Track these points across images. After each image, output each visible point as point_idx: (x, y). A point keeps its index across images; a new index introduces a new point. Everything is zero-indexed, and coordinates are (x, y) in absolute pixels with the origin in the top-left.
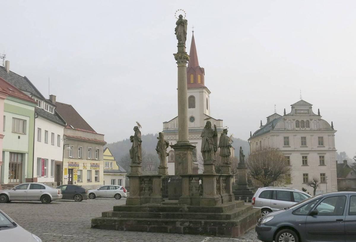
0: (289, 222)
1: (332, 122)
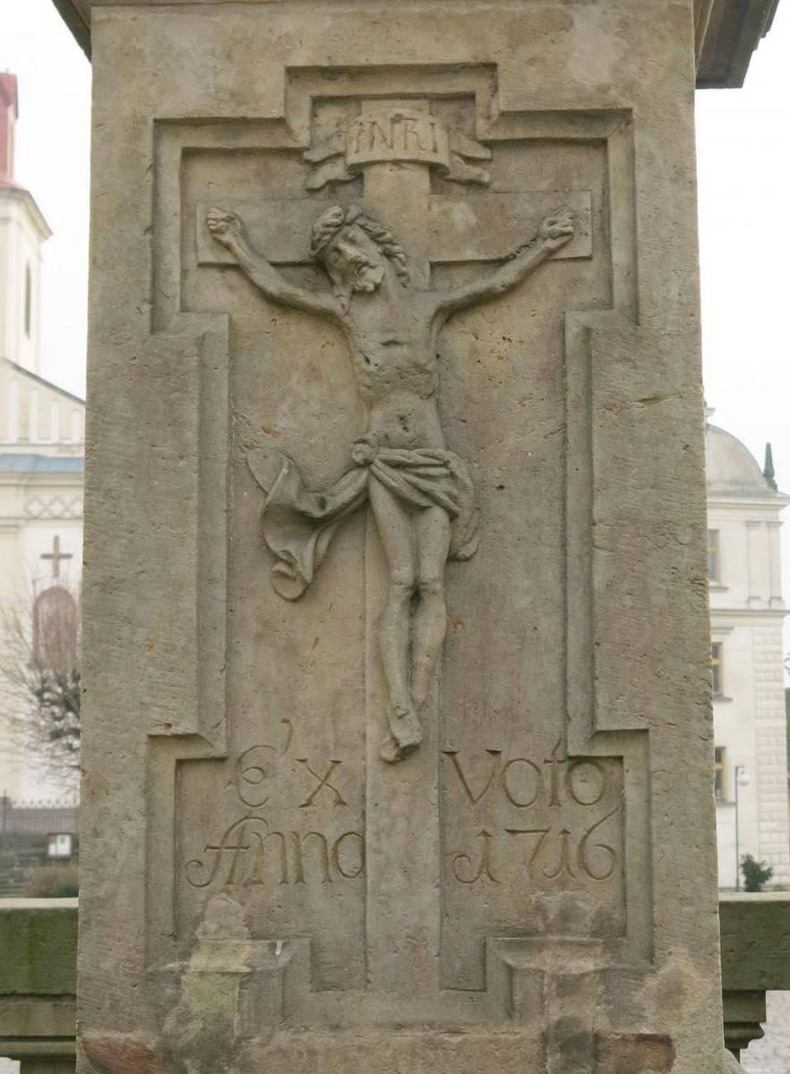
0: (406, 169)
1: (769, 447)
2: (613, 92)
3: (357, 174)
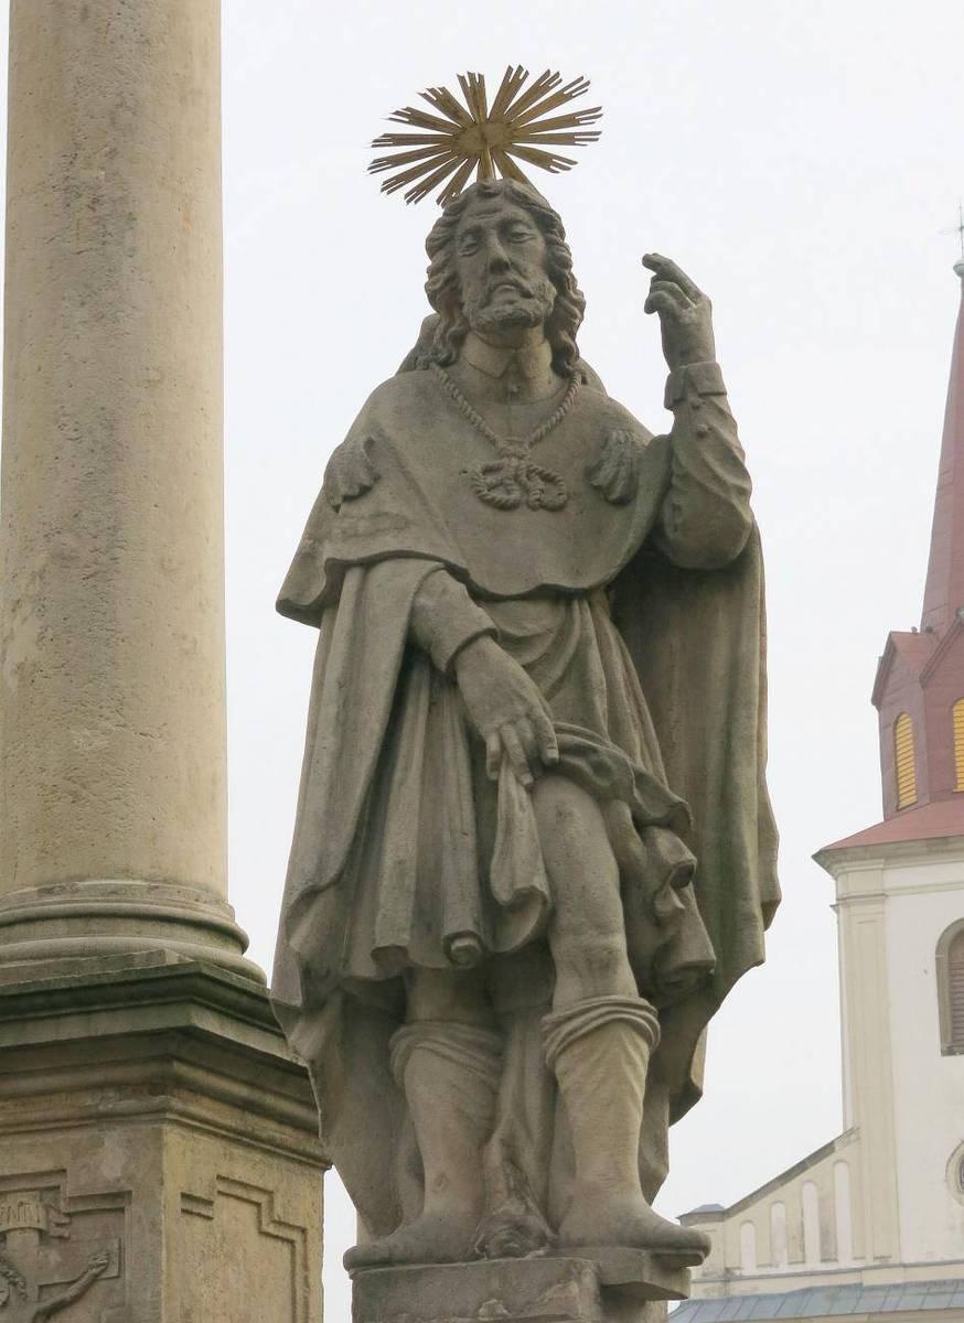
2: (123, 1182)
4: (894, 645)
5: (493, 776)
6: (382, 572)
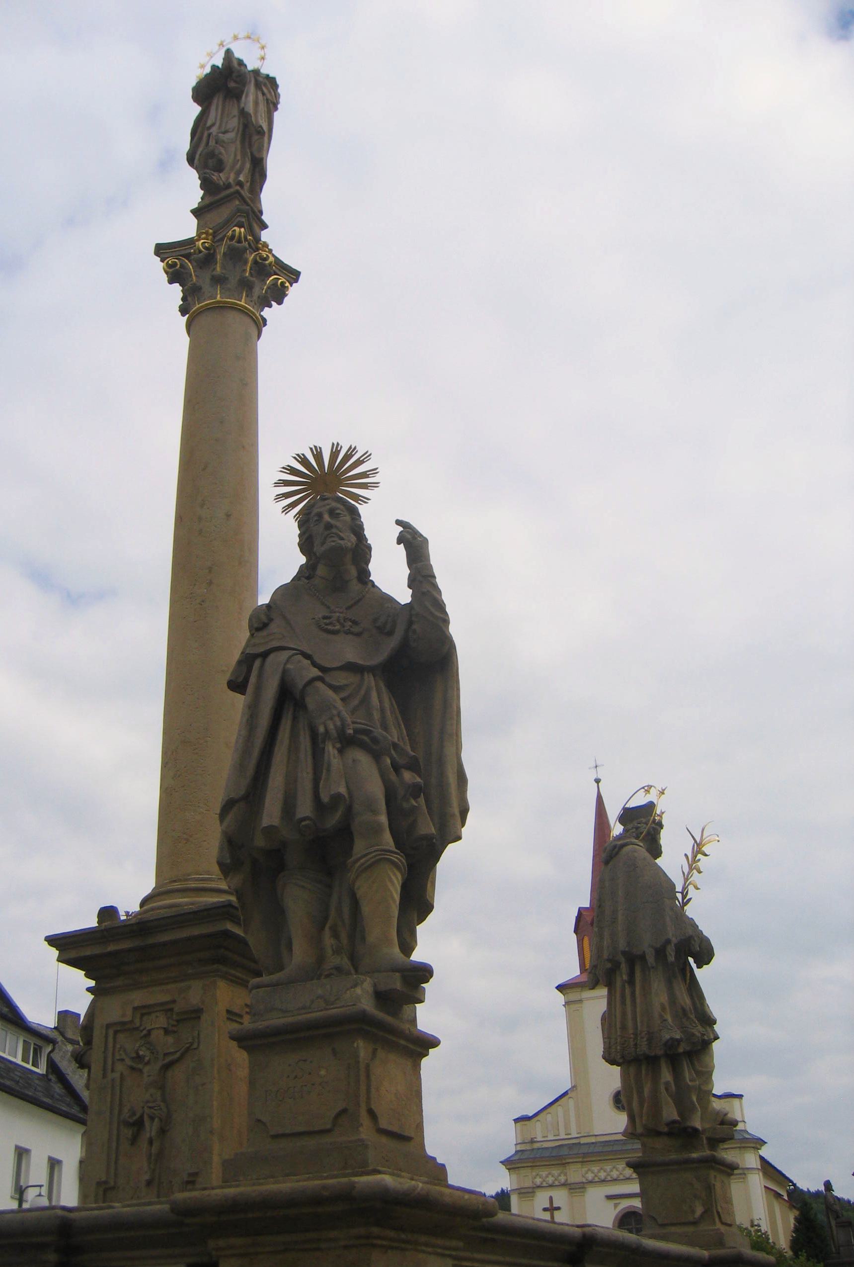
3: (149, 1031)
4: (581, 911)
5: (321, 746)
6: (271, 657)
